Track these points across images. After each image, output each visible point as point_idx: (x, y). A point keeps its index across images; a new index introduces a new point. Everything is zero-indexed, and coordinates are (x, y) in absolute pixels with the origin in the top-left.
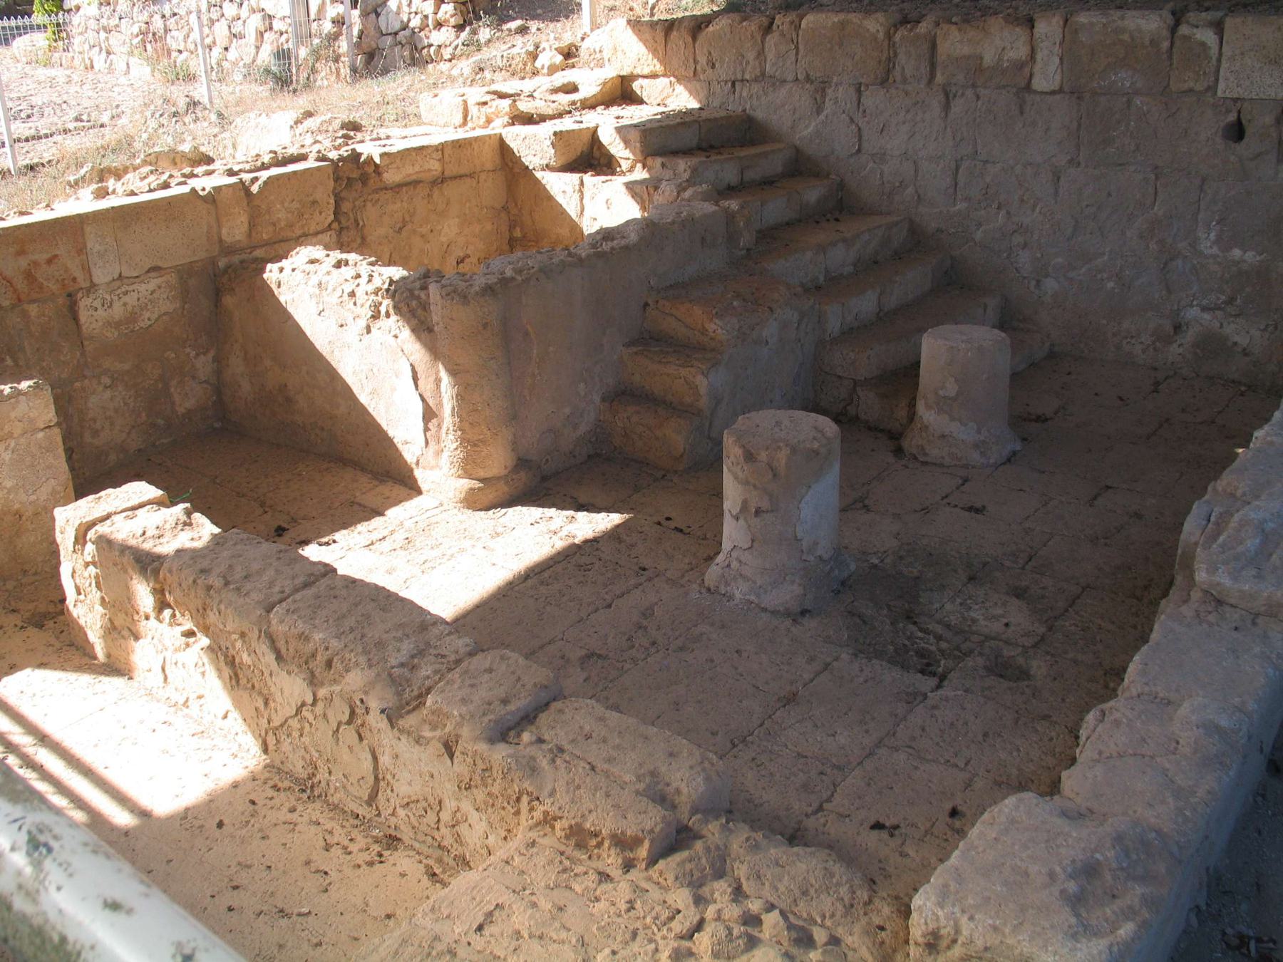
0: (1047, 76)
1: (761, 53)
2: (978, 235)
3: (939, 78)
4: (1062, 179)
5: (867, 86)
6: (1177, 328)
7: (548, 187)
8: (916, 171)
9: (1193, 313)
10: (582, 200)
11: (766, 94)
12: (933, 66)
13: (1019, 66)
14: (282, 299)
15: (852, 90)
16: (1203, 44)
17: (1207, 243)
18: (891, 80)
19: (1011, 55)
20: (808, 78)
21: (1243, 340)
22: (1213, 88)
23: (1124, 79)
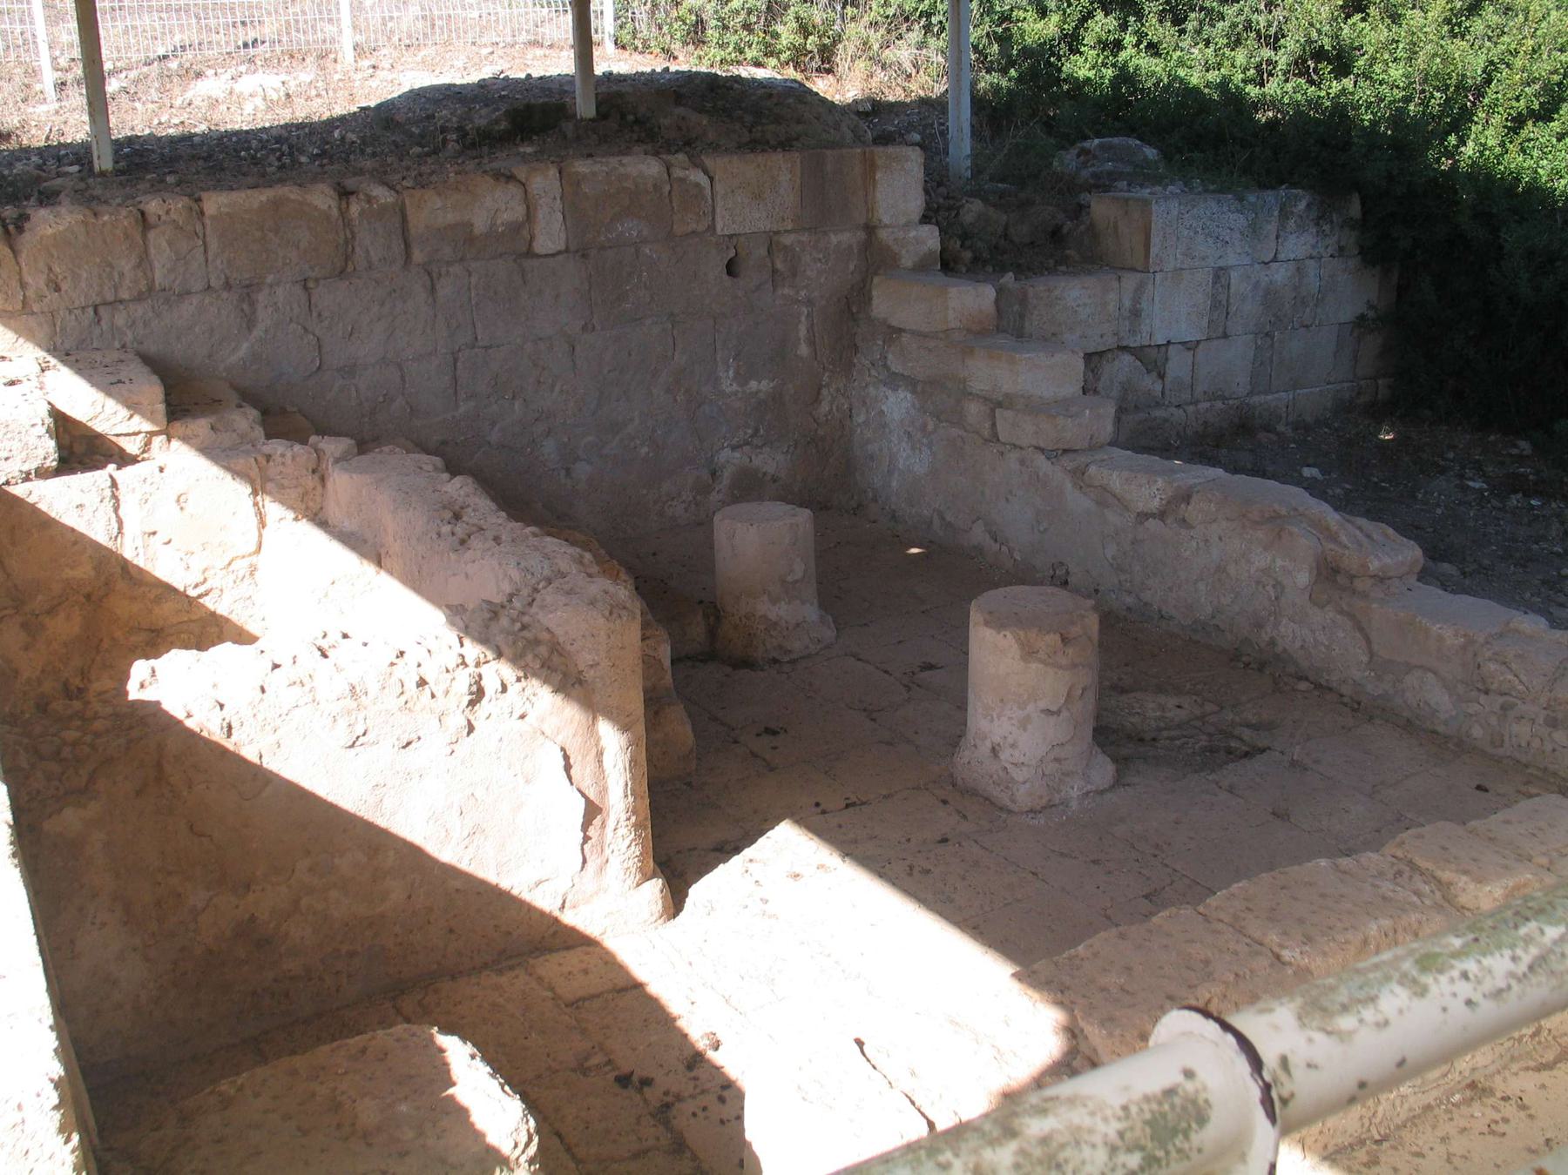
0: (550, 235)
1: (144, 260)
2: (494, 437)
3: (418, 256)
4: (578, 348)
5: (317, 280)
6: (713, 474)
7: (43, 506)
8: (403, 378)
9: (726, 453)
10: (116, 509)
11: (158, 315)
12: (407, 246)
13: (515, 228)
14: (249, 753)
15: (298, 290)
16: (697, 185)
17: (728, 385)
18: (350, 269)
19: (506, 217)
20: (228, 286)
21: (770, 469)
22: (712, 228)
23: (631, 228)
